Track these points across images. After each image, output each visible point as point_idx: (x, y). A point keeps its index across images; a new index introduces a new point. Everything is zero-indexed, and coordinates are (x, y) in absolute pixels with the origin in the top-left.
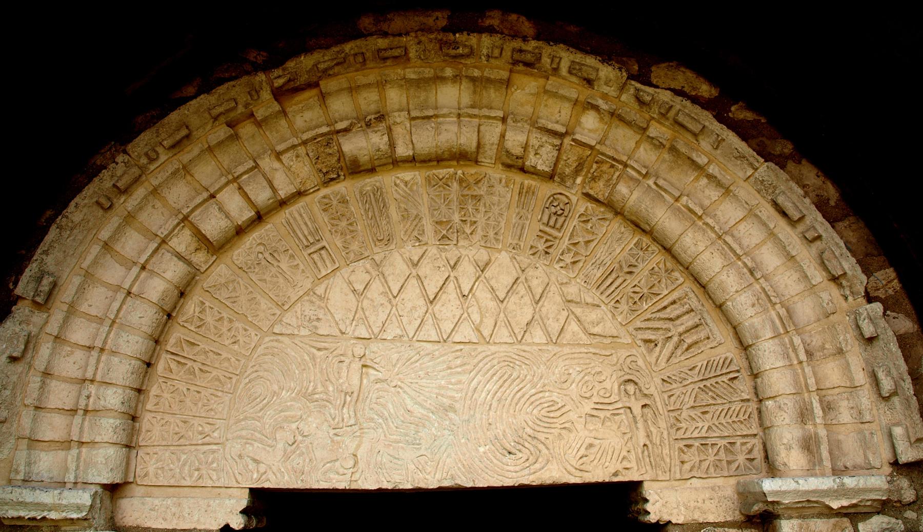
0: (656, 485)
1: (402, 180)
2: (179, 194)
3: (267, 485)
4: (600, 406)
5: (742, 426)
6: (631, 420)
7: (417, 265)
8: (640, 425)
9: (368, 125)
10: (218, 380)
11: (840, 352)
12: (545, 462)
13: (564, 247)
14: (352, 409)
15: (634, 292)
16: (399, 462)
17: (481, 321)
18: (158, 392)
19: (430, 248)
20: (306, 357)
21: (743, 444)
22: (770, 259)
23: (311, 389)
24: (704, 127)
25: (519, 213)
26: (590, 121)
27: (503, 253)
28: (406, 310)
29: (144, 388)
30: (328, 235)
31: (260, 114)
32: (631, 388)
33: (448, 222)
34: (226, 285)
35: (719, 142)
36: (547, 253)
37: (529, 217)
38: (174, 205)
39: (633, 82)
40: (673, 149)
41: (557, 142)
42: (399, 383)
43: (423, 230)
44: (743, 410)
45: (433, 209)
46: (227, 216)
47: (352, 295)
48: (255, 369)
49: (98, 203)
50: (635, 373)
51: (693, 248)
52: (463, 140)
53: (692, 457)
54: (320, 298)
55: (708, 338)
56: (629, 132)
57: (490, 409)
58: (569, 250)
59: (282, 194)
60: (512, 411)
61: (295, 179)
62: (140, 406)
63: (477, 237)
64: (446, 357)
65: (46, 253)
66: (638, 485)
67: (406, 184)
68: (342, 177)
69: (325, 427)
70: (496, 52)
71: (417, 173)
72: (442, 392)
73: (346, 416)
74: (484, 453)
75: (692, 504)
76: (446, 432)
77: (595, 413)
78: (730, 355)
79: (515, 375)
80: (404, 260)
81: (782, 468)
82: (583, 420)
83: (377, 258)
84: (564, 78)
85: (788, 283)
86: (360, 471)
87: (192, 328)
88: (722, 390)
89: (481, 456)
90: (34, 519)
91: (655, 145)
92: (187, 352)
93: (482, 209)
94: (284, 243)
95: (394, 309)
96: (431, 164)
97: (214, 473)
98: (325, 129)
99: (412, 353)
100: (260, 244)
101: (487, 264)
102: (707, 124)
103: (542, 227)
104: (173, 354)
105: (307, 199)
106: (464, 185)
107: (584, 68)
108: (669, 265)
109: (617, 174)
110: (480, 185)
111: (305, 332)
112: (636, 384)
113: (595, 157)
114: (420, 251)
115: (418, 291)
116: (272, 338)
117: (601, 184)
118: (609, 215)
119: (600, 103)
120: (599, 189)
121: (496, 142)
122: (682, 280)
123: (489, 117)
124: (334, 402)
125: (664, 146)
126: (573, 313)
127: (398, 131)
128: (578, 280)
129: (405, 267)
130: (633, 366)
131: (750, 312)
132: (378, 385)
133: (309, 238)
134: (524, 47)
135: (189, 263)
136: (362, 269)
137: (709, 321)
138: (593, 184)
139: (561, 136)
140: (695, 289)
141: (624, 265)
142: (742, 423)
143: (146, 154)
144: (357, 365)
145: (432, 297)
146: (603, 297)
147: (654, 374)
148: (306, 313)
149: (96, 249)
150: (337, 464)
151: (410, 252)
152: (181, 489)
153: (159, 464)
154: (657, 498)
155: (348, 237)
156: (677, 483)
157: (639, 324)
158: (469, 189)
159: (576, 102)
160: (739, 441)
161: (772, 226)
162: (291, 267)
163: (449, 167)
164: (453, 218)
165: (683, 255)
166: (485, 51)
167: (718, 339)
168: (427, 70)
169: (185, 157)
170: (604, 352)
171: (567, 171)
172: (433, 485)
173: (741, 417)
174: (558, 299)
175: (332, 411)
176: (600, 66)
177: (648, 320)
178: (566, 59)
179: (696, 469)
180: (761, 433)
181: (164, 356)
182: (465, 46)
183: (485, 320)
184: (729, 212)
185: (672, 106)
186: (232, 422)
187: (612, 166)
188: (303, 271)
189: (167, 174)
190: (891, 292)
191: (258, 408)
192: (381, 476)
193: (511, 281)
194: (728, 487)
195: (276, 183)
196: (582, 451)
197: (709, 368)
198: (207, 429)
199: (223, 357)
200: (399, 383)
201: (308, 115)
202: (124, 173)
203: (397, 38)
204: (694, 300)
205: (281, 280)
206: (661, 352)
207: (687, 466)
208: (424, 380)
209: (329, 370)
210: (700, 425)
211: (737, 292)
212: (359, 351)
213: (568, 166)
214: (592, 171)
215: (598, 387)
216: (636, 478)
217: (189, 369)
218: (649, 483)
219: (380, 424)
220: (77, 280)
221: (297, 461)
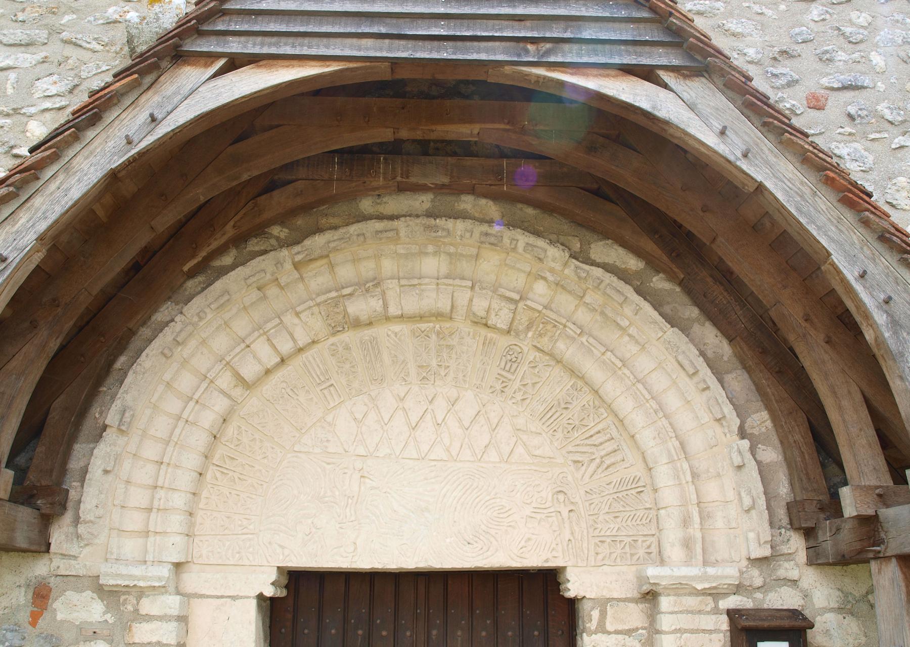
1: (393, 332)
9: (367, 291)
11: (719, 475)
21: (643, 541)
22: (673, 401)
24: (627, 298)
26: (540, 288)
31: (283, 281)
32: (561, 497)
33: (428, 366)
39: (574, 261)
40: (602, 313)
41: (513, 307)
49: (162, 353)
52: (440, 305)
54: (330, 424)
56: (570, 298)
58: (520, 389)
59: (301, 344)
65: (126, 392)
67: (396, 334)
77: (533, 515)
78: (639, 474)
81: (667, 560)
83: (373, 394)
87: (232, 446)
90: (127, 586)
93: (454, 356)
98: (334, 294)
102: (629, 295)
105: (319, 346)
106: (441, 336)
108: (597, 403)
110: (453, 336)
111: (317, 450)
118: (553, 363)
119: (548, 275)
120: (545, 343)
122: (606, 415)
123: (461, 286)
127: (391, 295)
134: (490, 231)
135: (229, 397)
139: (516, 302)
145: (414, 425)
146: (544, 427)
149: (161, 388)
156: (592, 569)
157: (570, 448)
160: (641, 539)
161: (674, 377)
163: (430, 322)
166: (459, 233)
169: (227, 316)
171: (521, 328)
182: (444, 229)
184: (644, 364)
187: (555, 326)
190: (763, 430)
194: (629, 572)
196: (523, 543)
201: (320, 280)
203: (391, 222)
206: (586, 470)
207: (600, 557)
212: (359, 465)
220: (148, 412)
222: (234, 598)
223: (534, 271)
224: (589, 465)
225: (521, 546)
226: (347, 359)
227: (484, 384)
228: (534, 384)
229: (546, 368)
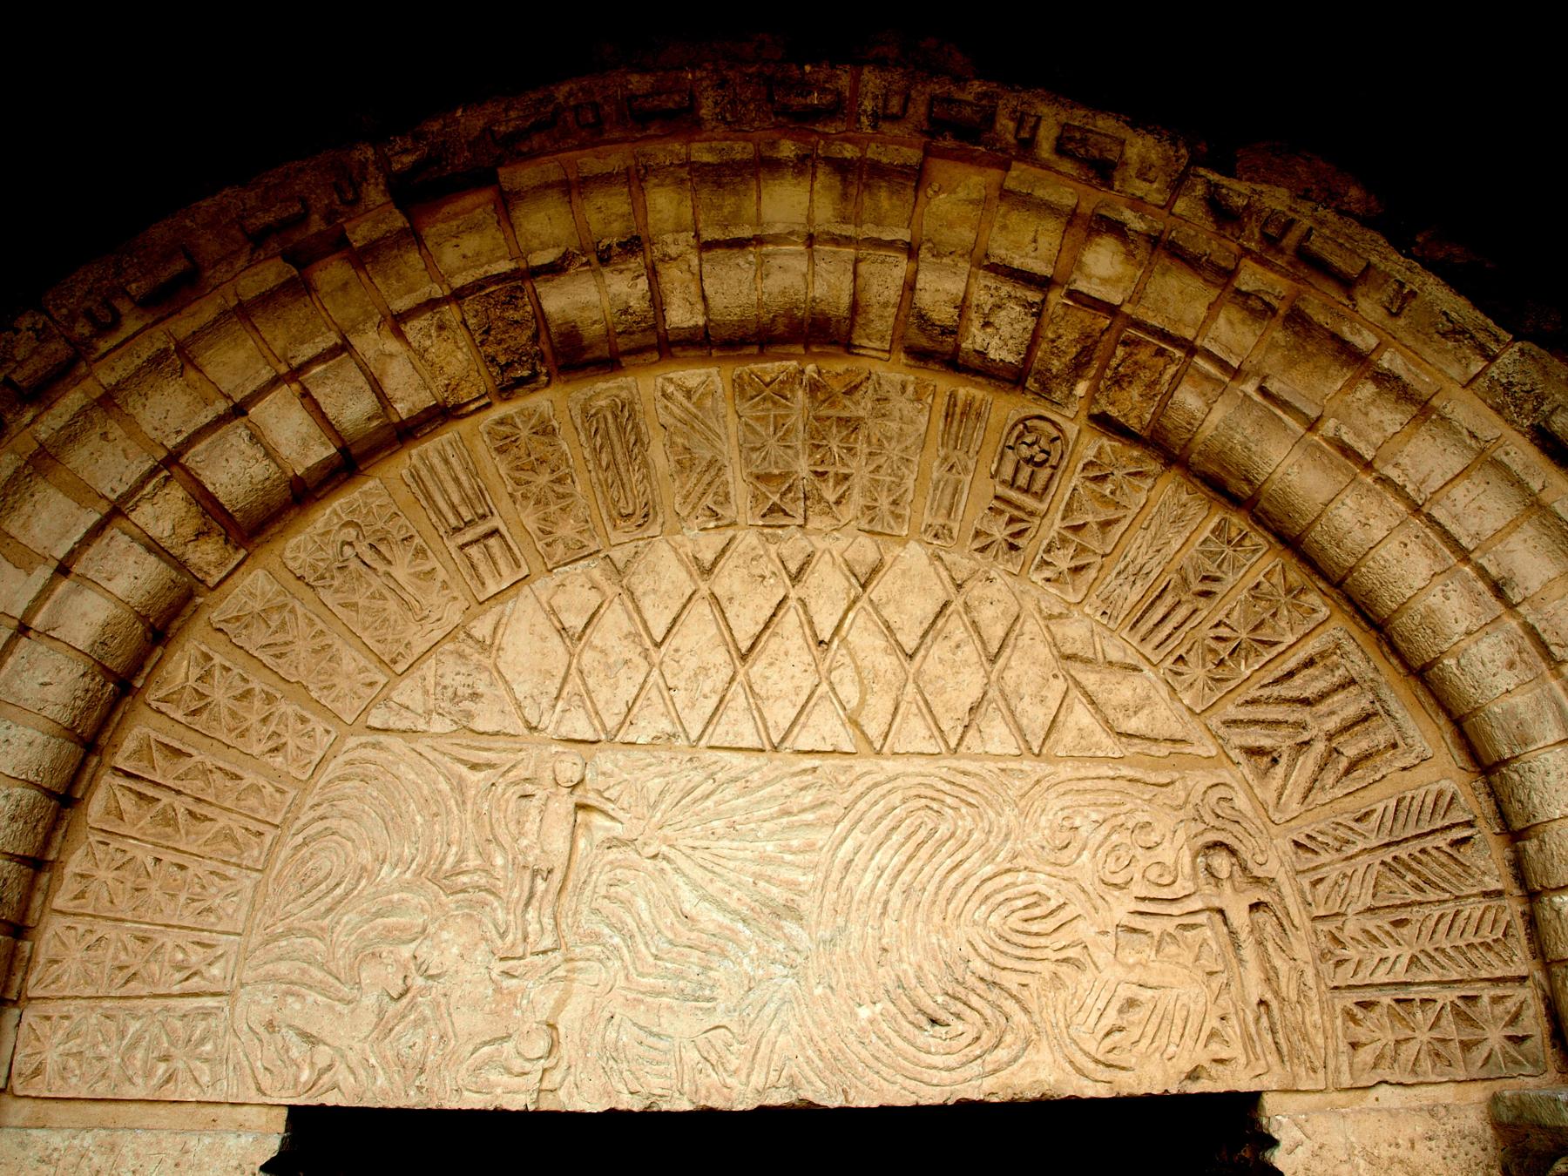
0: (1291, 1102)
1: (679, 387)
2: (167, 410)
3: (331, 1100)
4: (1149, 906)
5: (1490, 956)
6: (1227, 940)
7: (710, 571)
8: (1249, 952)
10: (229, 836)
12: (1020, 1044)
13: (1053, 533)
14: (548, 911)
15: (1218, 638)
16: (662, 1045)
17: (863, 702)
18: (85, 867)
19: (741, 535)
20: (444, 786)
21: (1496, 1000)
23: (451, 860)
25: (946, 459)
27: (913, 545)
28: (685, 675)
29: (52, 856)
30: (506, 504)
31: (360, 234)
32: (1221, 862)
33: (784, 476)
34: (263, 616)
35: (1405, 299)
36: (1013, 547)
37: (971, 465)
38: (153, 434)
39: (1202, 171)
40: (1297, 320)
41: (1034, 296)
42: (664, 849)
43: (727, 495)
44: (1490, 916)
45: (749, 449)
46: (270, 454)
47: (557, 639)
48: (320, 811)
50: (1230, 826)
51: (1358, 534)
52: (819, 290)
53: (1378, 1031)
54: (483, 646)
55: (1395, 746)
56: (1194, 284)
57: (884, 913)
59: (403, 409)
60: (937, 918)
61: (434, 378)
62: (38, 898)
63: (849, 511)
64: (778, 786)
66: (1250, 1101)
67: (688, 394)
68: (544, 379)
69: (480, 955)
70: (895, 104)
71: (714, 370)
72: (769, 870)
73: (533, 928)
74: (872, 1021)
75: (1385, 1152)
76: (778, 970)
77: (1138, 922)
78: (1449, 786)
79: (943, 830)
80: (681, 561)
82: (1109, 940)
83: (616, 554)
84: (1046, 166)
86: (564, 1065)
87: (179, 716)
88: (1438, 869)
89: (863, 1030)
91: (1252, 311)
93: (862, 448)
94: (403, 520)
95: (655, 672)
96: (747, 351)
97: (206, 1067)
98: (505, 266)
99: (697, 777)
101: (875, 571)
102: (1374, 259)
103: (1001, 490)
104: (128, 775)
105: (464, 426)
107: (1093, 138)
109: (1172, 369)
110: (858, 395)
111: (440, 725)
112: (1233, 852)
113: (1120, 332)
114: (718, 540)
115: (713, 630)
116: (363, 739)
117: (1135, 392)
118: (1153, 466)
119: (1128, 216)
120: (1131, 405)
121: (895, 299)
122: (1324, 612)
123: (878, 244)
124: (504, 895)
125: (1274, 311)
126: (1077, 684)
127: (673, 276)
128: (1087, 610)
129: (683, 575)
131: (1505, 680)
132: (613, 854)
133: (463, 510)
136: (582, 579)
137: (1393, 706)
138: (1115, 393)
139: (1043, 283)
140: (1356, 632)
142: (1489, 947)
143: (89, 315)
144: (563, 804)
145: (744, 645)
146: (1147, 649)
147: (1274, 830)
148: (446, 681)
150: (508, 1047)
151: (694, 541)
152: (122, 1108)
153: (73, 1045)
154: (1299, 1135)
155: (553, 508)
156: (1341, 1098)
157: (1232, 712)
158: (833, 405)
159: (1072, 218)
160: (1487, 993)
161: (1536, 485)
162: (417, 575)
164: (796, 468)
165: (1333, 551)
166: (868, 105)
167: (1418, 749)
168: (738, 146)
169: (183, 326)
170: (1153, 778)
171: (1056, 365)
172: (744, 1101)
173: (1487, 935)
174: (1043, 652)
175: (500, 915)
176: (1127, 134)
178: (1051, 121)
179: (1386, 1063)
180: (1539, 975)
183: (871, 700)
184: (1427, 460)
186: (255, 940)
187: (1160, 352)
188: (445, 586)
189: (138, 362)
191: (321, 906)
192: (615, 1079)
193: (932, 608)
195: (389, 385)
197: (1402, 817)
198: (196, 956)
199: (245, 784)
200: (664, 849)
201: (471, 243)
202: (35, 351)
204: (1357, 657)
205: (392, 605)
206: (1287, 777)
207: (1365, 1055)
208: (725, 843)
209: (495, 815)
210: (1392, 952)
211: (1469, 633)
212: (569, 770)
213: (1057, 353)
214: (1114, 363)
215: (1143, 859)
216: (1244, 1084)
217: (164, 811)
218: (1277, 1097)
219: (617, 948)
221: (410, 1040)
224: (1293, 762)
226: (542, 461)
227: (956, 527)
228: (1106, 525)
229: (1135, 481)
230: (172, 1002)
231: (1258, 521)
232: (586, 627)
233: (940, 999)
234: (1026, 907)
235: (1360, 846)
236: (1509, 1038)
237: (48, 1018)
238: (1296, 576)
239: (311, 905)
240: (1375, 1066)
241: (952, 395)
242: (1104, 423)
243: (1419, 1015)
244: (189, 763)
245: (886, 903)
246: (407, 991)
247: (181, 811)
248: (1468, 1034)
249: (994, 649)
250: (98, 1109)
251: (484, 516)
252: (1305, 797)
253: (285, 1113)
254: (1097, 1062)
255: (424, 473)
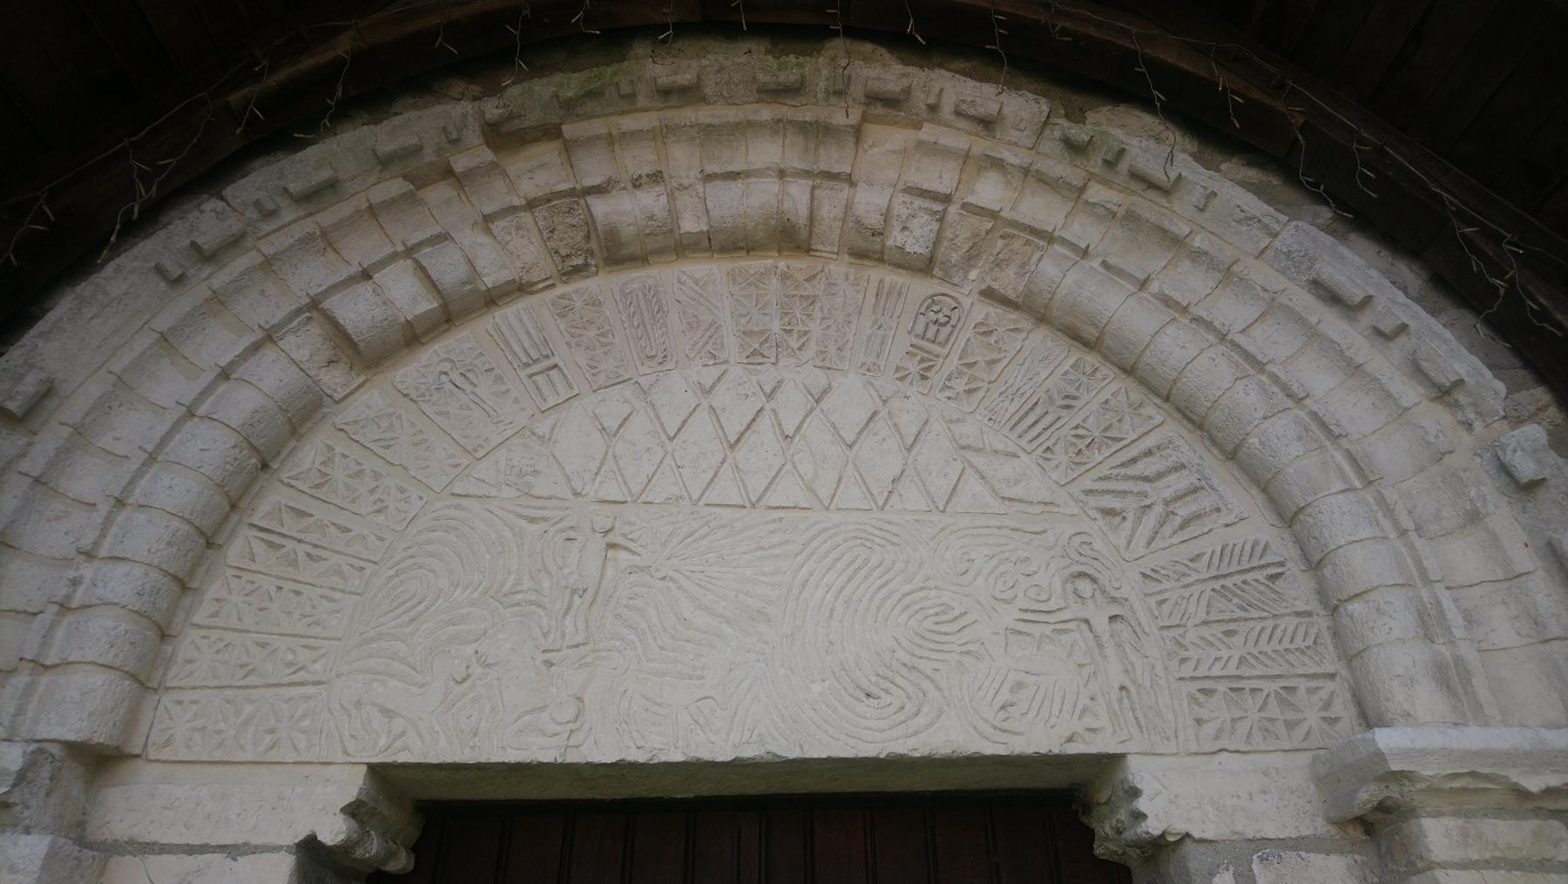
2: (312, 275)
3: (402, 758)
4: (1031, 615)
5: (1305, 659)
7: (709, 392)
8: (1110, 650)
11: (1474, 518)
15: (1077, 436)
20: (508, 533)
23: (510, 583)
25: (876, 322)
32: (1085, 587)
33: (762, 332)
36: (924, 378)
48: (410, 552)
50: (1091, 562)
57: (831, 617)
58: (961, 373)
67: (697, 282)
73: (569, 630)
74: (821, 694)
79: (875, 560)
83: (642, 381)
84: (947, 125)
85: (1353, 411)
92: (290, 525)
100: (446, 360)
101: (825, 392)
103: (914, 341)
110: (815, 282)
112: (1094, 580)
114: (715, 372)
117: (1011, 271)
118: (1026, 324)
120: (1008, 281)
126: (972, 465)
127: (685, 201)
130: (1085, 549)
131: (1296, 449)
132: (634, 578)
137: (1215, 483)
139: (946, 199)
140: (1185, 433)
141: (1055, 396)
142: (1303, 652)
144: (599, 542)
145: (732, 439)
152: (233, 768)
153: (199, 723)
156: (1192, 761)
158: (797, 287)
160: (1303, 685)
169: (327, 218)
171: (955, 257)
177: (1105, 478)
180: (1344, 672)
181: (245, 532)
185: (1122, 151)
188: (516, 400)
191: (405, 618)
196: (1004, 696)
197: (1226, 558)
198: (304, 656)
206: (1134, 531)
207: (1209, 730)
210: (1224, 653)
216: (1112, 748)
222: (233, 851)
223: (976, 151)
225: (1000, 700)
229: (1013, 335)
230: (282, 690)
231: (1105, 358)
232: (621, 426)
233: (873, 679)
234: (936, 614)
235: (1195, 577)
236: (1325, 719)
237: (180, 703)
238: (1137, 394)
239: (398, 617)
240: (1217, 738)
241: (881, 281)
242: (988, 294)
243: (1250, 701)
244: (311, 520)
245: (832, 610)
246: (469, 676)
247: (301, 555)
248: (1290, 716)
249: (910, 441)
250: (214, 769)
251: (547, 357)
252: (1149, 544)
253: (365, 768)
254: (995, 728)
255: (504, 329)
